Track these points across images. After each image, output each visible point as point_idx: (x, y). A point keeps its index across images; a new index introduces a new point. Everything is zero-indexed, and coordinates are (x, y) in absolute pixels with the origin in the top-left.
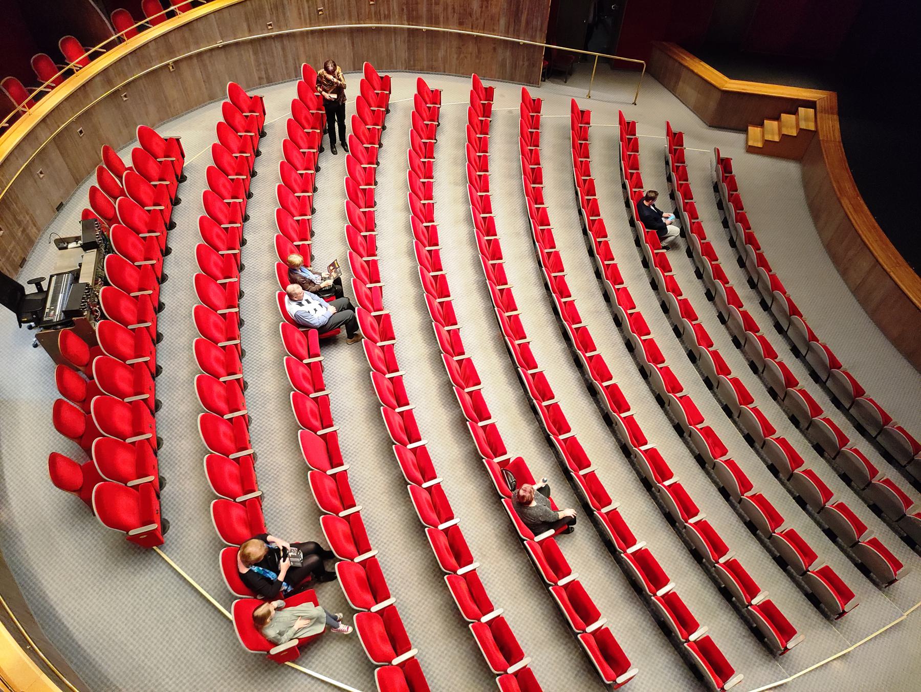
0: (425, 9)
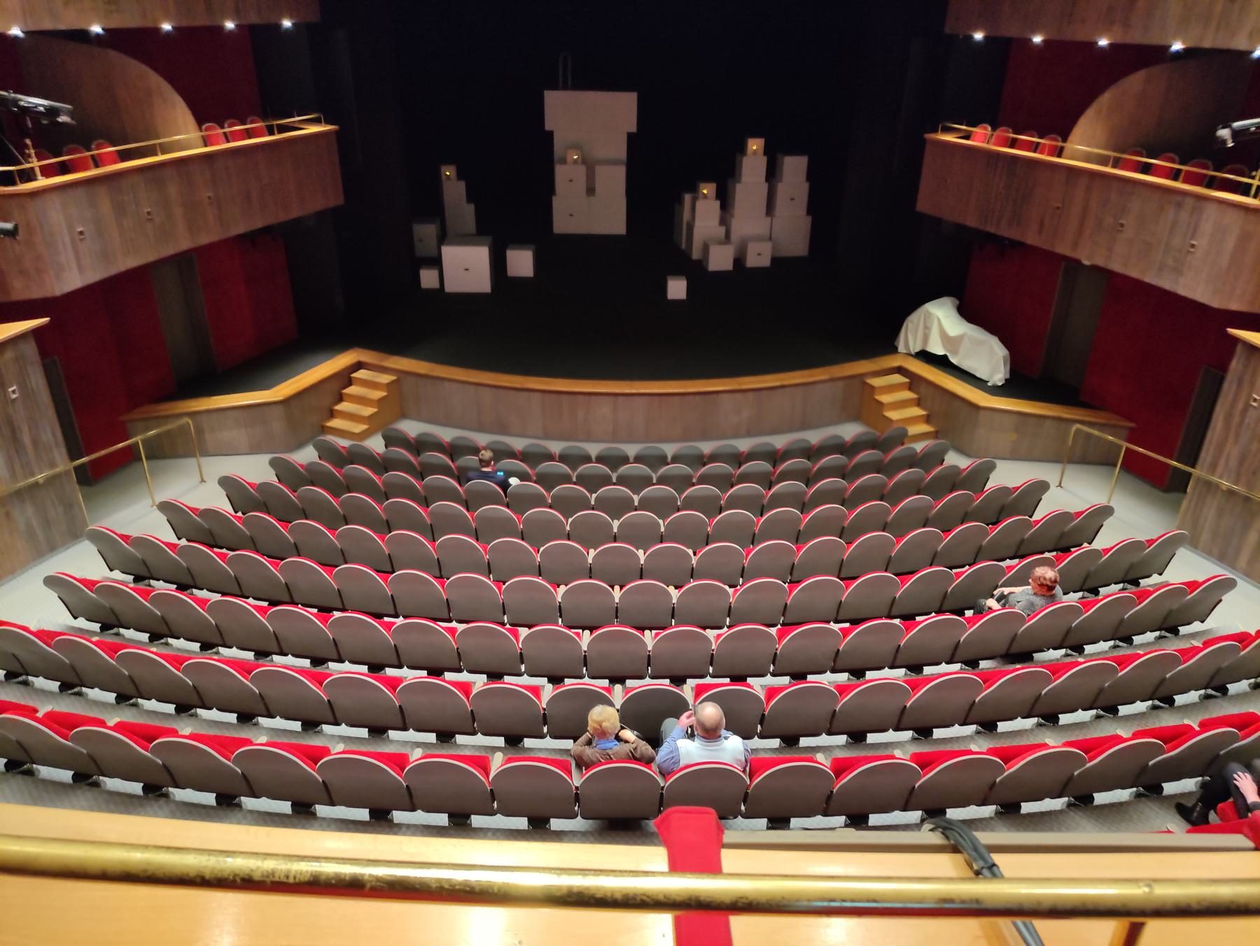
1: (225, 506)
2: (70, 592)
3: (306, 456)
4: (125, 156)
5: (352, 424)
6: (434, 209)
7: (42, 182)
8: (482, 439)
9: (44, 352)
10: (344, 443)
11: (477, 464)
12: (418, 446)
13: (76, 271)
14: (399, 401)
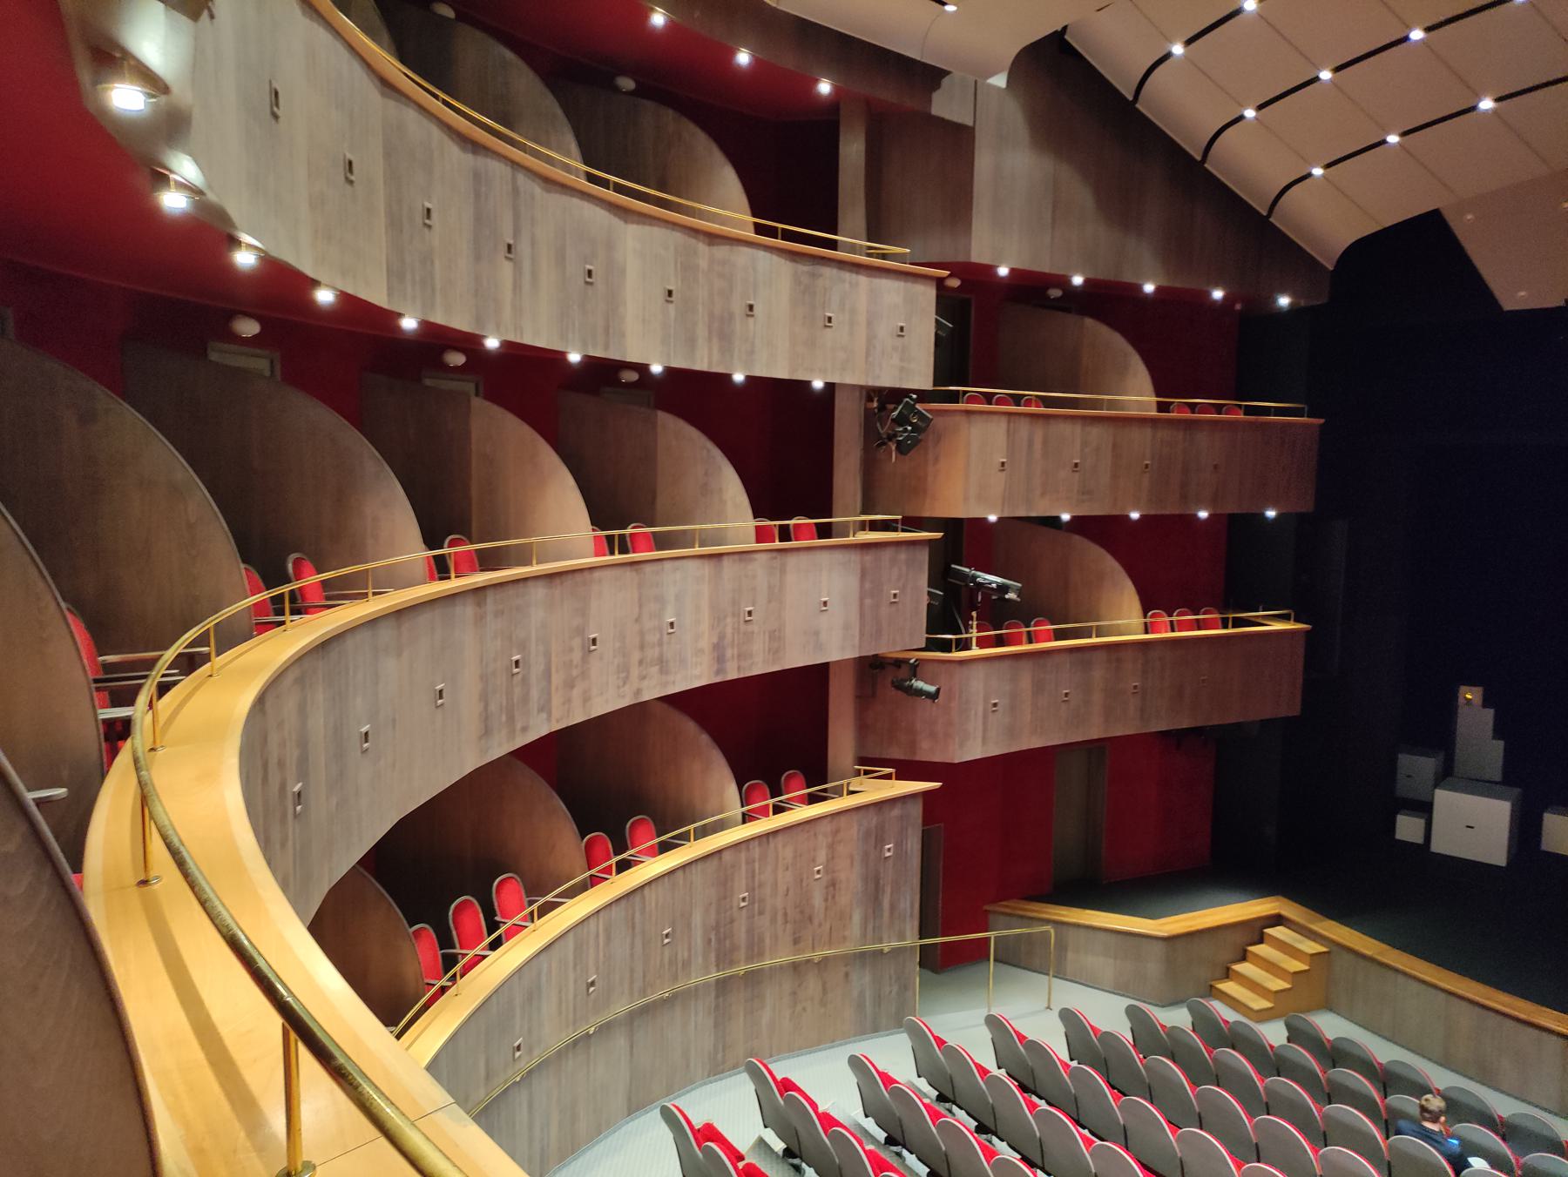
0: (743, 929)
1: (1059, 1049)
2: (877, 1089)
3: (1178, 1018)
4: (1060, 635)
5: (1251, 996)
6: (1437, 735)
7: (976, 652)
8: (1442, 1078)
9: (928, 818)
10: (1230, 1015)
11: (1415, 1111)
12: (1336, 1054)
13: (979, 740)
14: (1320, 983)
